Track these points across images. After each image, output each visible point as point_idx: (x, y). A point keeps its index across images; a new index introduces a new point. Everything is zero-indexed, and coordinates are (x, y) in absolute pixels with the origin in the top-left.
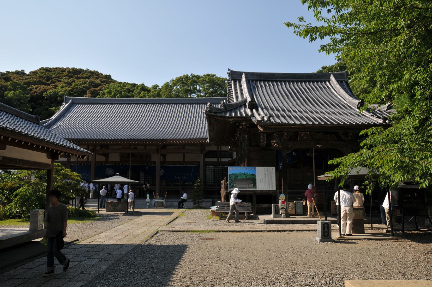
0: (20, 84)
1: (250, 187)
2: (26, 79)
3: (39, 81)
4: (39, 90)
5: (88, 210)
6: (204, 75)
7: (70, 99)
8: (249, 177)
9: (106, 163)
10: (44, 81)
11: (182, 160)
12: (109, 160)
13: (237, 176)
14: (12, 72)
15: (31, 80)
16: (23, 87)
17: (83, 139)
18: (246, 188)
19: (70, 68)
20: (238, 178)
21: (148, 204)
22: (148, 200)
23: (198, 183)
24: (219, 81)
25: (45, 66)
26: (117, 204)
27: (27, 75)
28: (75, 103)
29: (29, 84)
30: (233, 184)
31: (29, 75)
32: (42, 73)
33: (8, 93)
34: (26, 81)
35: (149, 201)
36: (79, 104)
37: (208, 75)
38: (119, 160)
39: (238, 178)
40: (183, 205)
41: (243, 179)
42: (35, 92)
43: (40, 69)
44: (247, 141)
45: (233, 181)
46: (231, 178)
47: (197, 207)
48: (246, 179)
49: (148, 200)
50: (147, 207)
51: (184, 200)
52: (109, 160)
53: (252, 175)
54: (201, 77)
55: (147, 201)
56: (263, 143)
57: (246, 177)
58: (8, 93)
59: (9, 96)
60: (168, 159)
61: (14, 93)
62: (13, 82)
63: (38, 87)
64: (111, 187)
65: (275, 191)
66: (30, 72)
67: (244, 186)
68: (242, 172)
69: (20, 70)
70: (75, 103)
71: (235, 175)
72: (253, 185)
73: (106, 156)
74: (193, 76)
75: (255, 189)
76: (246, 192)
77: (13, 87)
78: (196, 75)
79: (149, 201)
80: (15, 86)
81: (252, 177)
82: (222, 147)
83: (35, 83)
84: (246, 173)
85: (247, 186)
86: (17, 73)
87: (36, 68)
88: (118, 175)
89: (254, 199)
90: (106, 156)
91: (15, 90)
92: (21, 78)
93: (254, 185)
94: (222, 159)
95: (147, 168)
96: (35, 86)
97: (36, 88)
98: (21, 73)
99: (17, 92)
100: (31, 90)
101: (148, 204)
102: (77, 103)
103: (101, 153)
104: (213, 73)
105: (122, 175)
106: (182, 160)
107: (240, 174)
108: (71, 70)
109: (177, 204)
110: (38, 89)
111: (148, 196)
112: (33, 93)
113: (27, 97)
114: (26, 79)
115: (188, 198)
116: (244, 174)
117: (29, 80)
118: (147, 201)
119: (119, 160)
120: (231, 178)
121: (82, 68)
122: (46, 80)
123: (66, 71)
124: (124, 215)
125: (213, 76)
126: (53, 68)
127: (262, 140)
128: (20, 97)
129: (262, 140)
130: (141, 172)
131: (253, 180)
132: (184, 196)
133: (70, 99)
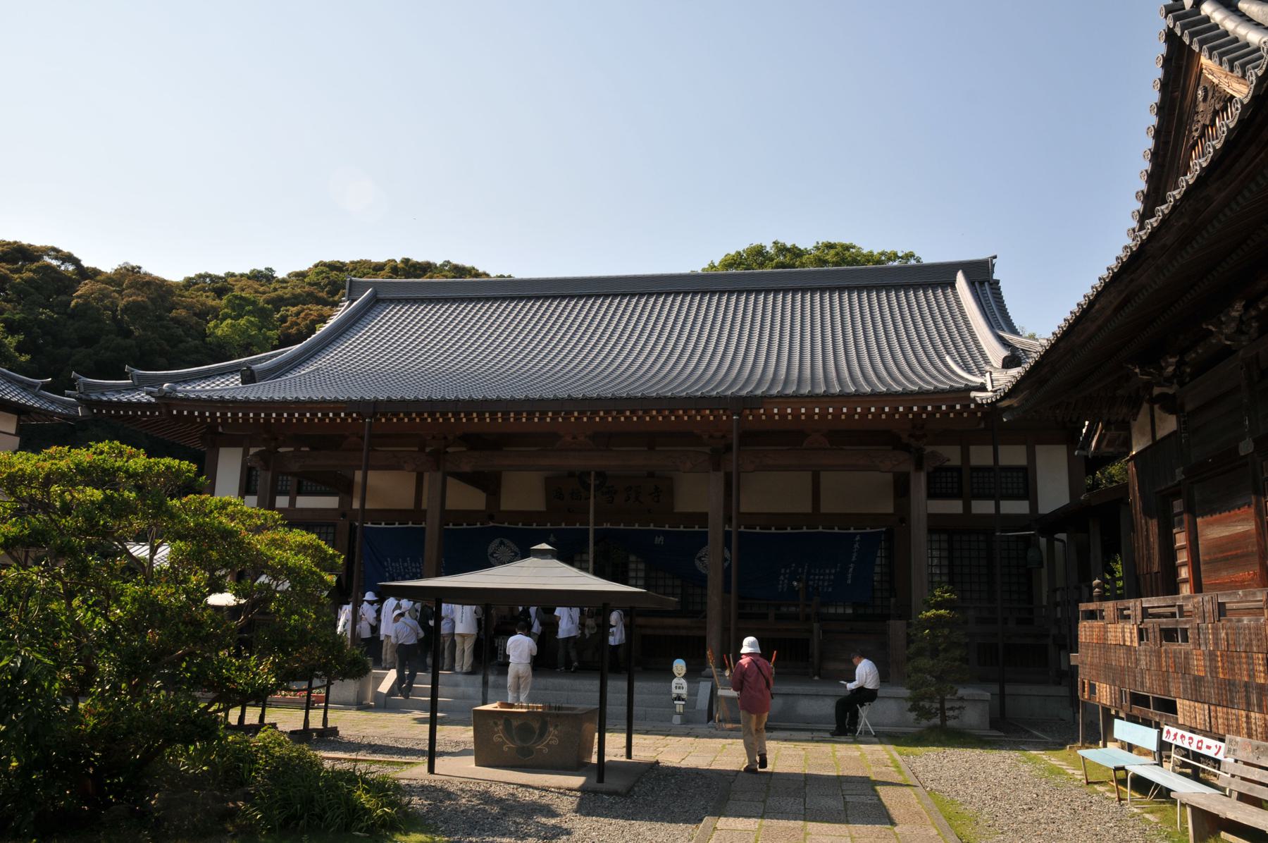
0: (254, 303)
2: (275, 290)
3: (310, 294)
4: (304, 319)
5: (351, 778)
6: (817, 248)
7: (366, 286)
9: (491, 518)
10: (323, 295)
11: (807, 509)
12: (503, 508)
14: (242, 275)
15: (287, 293)
16: (263, 310)
17: (390, 401)
19: (398, 260)
21: (679, 705)
22: (679, 685)
23: (938, 606)
24: (869, 261)
25: (327, 259)
26: (536, 725)
27: (279, 281)
28: (383, 300)
29: (278, 302)
31: (283, 281)
32: (318, 274)
33: (216, 326)
34: (273, 295)
35: (684, 692)
36: (399, 301)
37: (830, 246)
38: (542, 508)
40: (855, 717)
42: (295, 324)
43: (316, 266)
47: (932, 729)
49: (679, 685)
50: (677, 719)
51: (864, 696)
52: (503, 508)
55: (675, 691)
58: (216, 326)
59: (219, 332)
60: (749, 503)
61: (233, 325)
62: (236, 297)
63: (303, 310)
64: (503, 614)
66: (289, 275)
69: (261, 267)
70: (383, 300)
73: (488, 483)
74: (782, 249)
77: (233, 309)
78: (789, 245)
79: (684, 692)
80: (240, 307)
83: (295, 300)
86: (256, 276)
87: (305, 265)
88: (542, 554)
90: (488, 483)
91: (236, 318)
92: (261, 289)
94: (1002, 503)
95: (659, 540)
96: (294, 309)
97: (298, 314)
98: (263, 277)
99: (242, 322)
100: (283, 319)
101: (679, 705)
102: (391, 301)
103: (466, 468)
104: (847, 241)
105: (568, 554)
106: (807, 509)
108: (401, 265)
109: (827, 707)
110: (302, 315)
111: (679, 666)
112: (289, 328)
113: (269, 338)
114: (275, 290)
117: (280, 292)
118: (675, 691)
119: (542, 508)
121: (432, 260)
122: (328, 293)
123: (387, 269)
124: (584, 809)
125: (847, 248)
126: (352, 263)
128: (250, 336)
130: (632, 558)
132: (865, 672)
133: (366, 286)
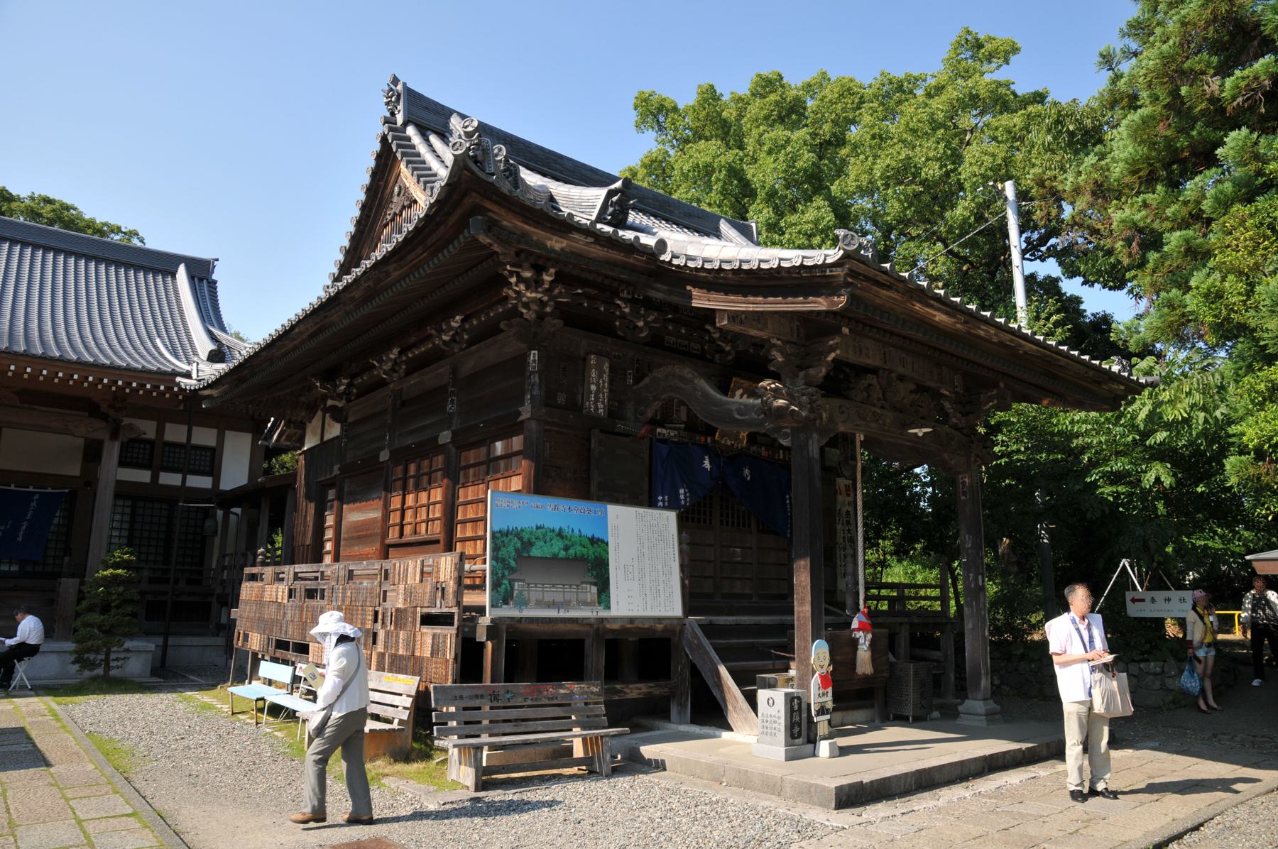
1: (586, 604)
6: (32, 198)
8: (577, 550)
13: (531, 544)
18: (566, 604)
20: (535, 552)
23: (116, 566)
30: (511, 582)
39: (535, 552)
41: (555, 558)
44: (536, 379)
45: (512, 570)
46: (503, 553)
47: (94, 679)
48: (567, 559)
53: (594, 541)
54: (19, 199)
56: (597, 400)
57: (566, 549)
65: (678, 619)
67: (559, 598)
68: (549, 524)
71: (518, 534)
72: (594, 589)
75: (603, 614)
76: (561, 627)
81: (590, 551)
82: (195, 429)
84: (567, 532)
85: (571, 595)
89: (596, 659)
93: (600, 592)
107: (544, 534)
115: (49, 633)
116: (560, 534)
120: (503, 553)
125: (67, 208)
127: (593, 387)
129: (593, 387)
131: (592, 565)
